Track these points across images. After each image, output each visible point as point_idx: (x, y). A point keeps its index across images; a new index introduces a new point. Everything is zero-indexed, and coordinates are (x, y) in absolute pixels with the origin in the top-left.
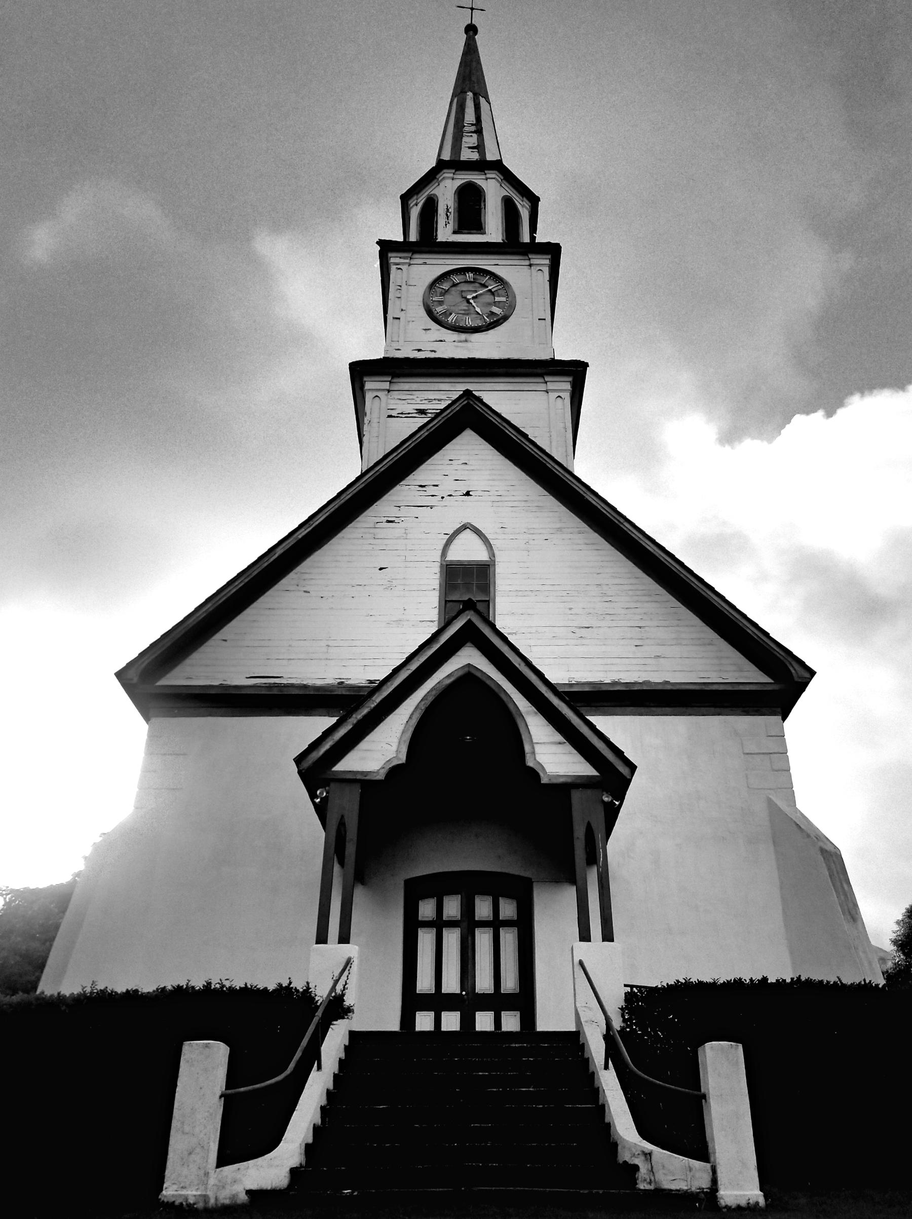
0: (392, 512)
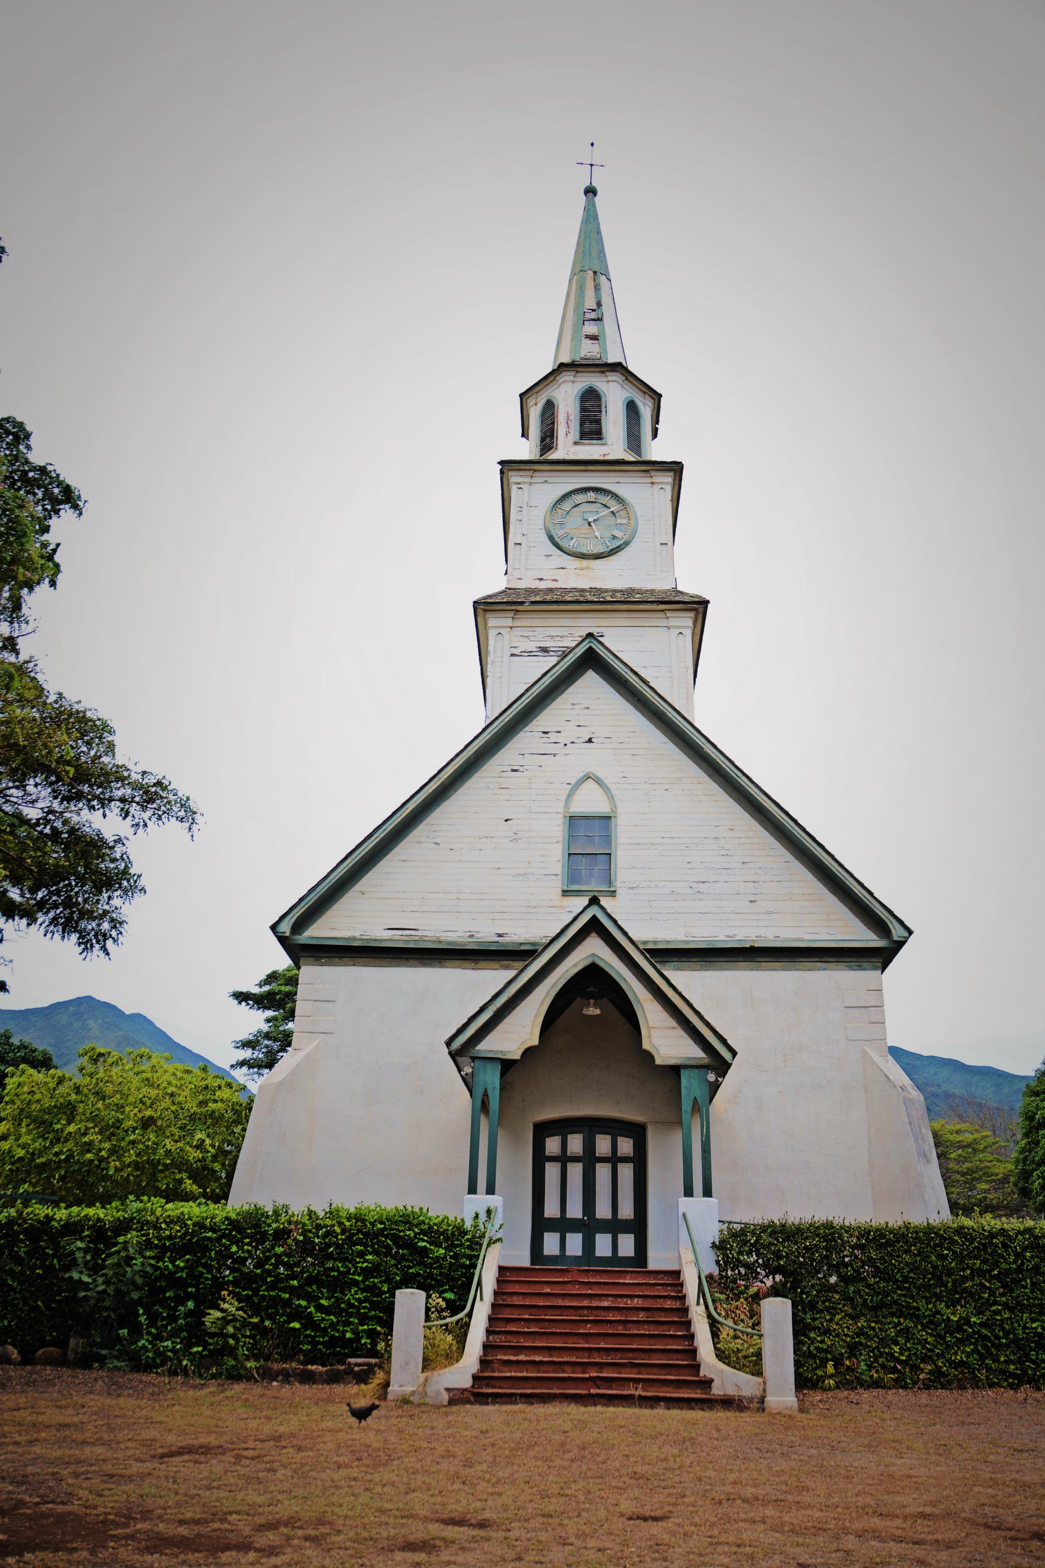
0: (517, 761)
